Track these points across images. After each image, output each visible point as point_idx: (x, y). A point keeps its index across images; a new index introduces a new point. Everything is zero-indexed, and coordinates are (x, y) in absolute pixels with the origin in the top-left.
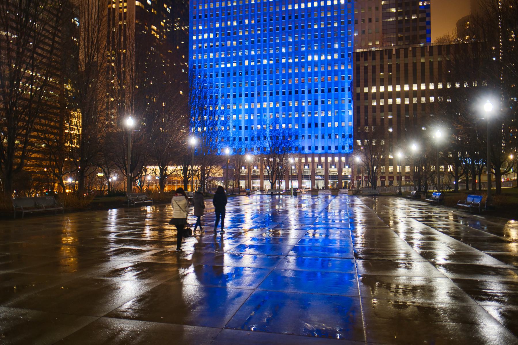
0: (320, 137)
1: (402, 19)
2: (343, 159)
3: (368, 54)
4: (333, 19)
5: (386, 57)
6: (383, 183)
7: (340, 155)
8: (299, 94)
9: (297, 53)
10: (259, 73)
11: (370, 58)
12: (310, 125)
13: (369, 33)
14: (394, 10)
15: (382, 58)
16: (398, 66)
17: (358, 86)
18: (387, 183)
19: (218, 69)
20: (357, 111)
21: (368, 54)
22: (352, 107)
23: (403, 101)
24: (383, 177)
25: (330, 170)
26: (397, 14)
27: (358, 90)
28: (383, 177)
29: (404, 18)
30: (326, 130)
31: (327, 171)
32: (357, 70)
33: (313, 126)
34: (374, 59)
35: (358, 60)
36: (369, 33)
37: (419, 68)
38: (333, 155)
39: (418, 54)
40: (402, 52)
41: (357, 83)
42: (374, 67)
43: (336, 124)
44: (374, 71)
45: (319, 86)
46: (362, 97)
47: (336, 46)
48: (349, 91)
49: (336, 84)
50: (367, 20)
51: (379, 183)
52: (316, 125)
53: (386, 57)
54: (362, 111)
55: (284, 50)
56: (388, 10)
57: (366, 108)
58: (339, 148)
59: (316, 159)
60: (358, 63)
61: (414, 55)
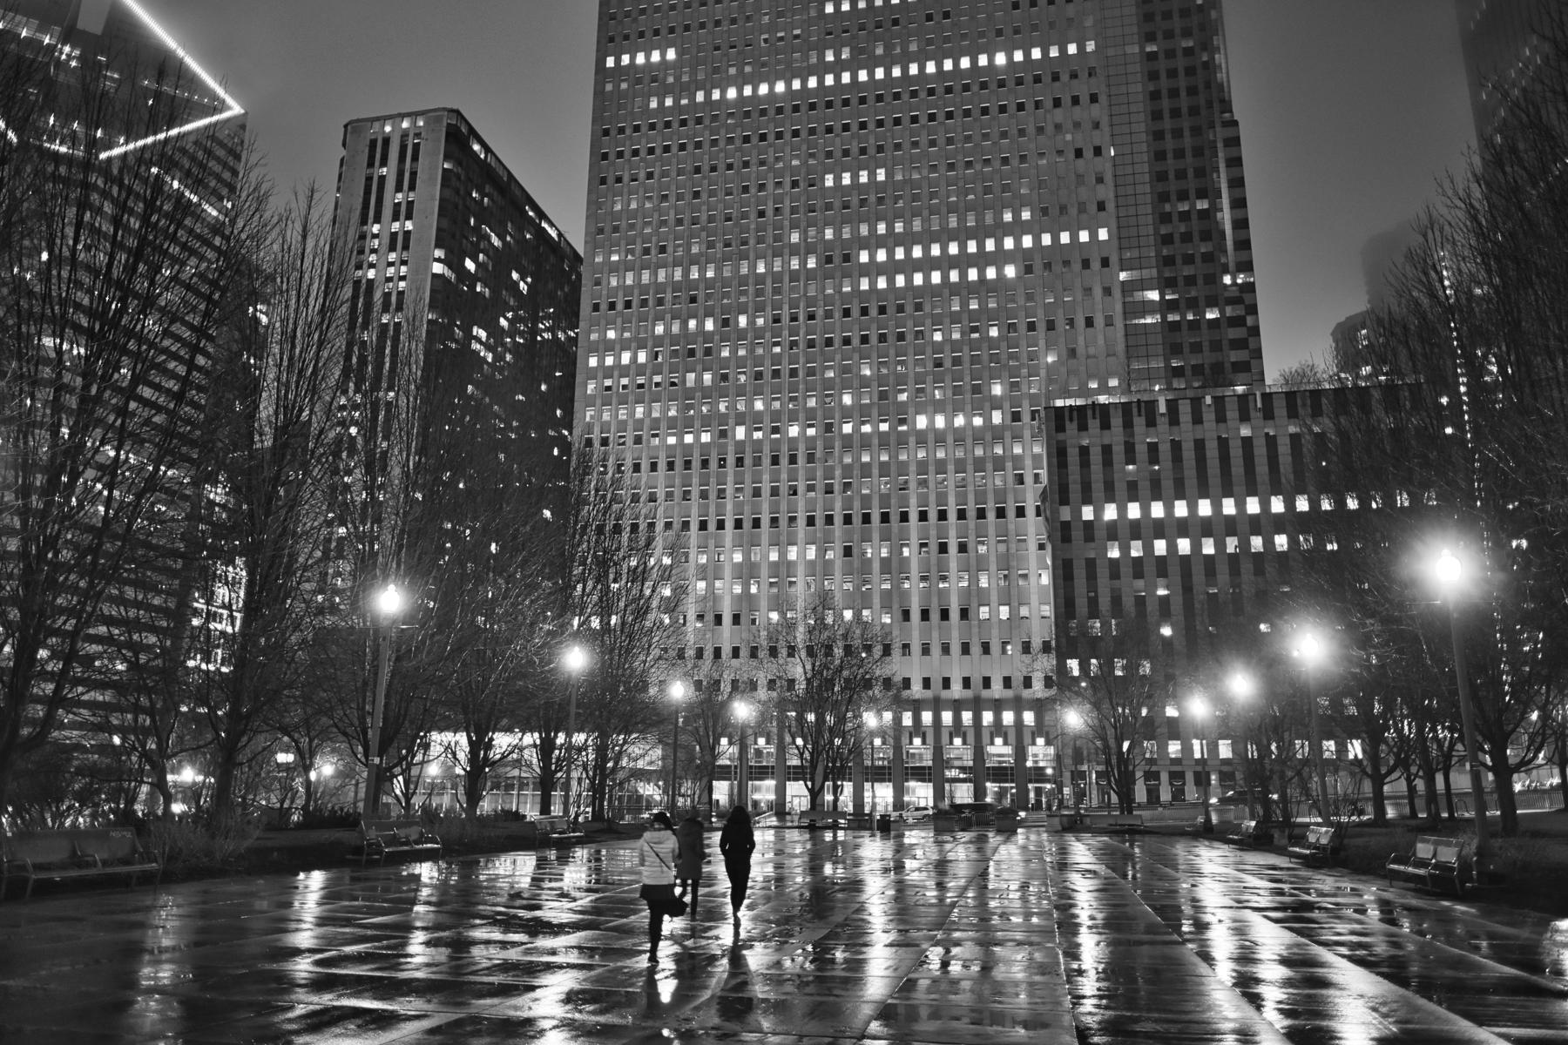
0: (956, 648)
1: (1177, 318)
2: (1029, 717)
3: (1090, 413)
4: (986, 316)
5: (1139, 422)
6: (1153, 794)
7: (1018, 705)
8: (892, 519)
9: (885, 406)
10: (775, 461)
11: (1093, 424)
12: (925, 615)
13: (1088, 357)
14: (1154, 295)
15: (1128, 425)
16: (1176, 446)
17: (1064, 501)
18: (1165, 795)
19: (657, 447)
20: (1064, 573)
21: (1090, 413)
22: (1049, 562)
23: (1197, 546)
24: (1152, 776)
25: (990, 749)
26: (1165, 307)
27: (1065, 514)
28: (1152, 776)
29: (1183, 316)
30: (975, 630)
31: (979, 753)
32: (1059, 455)
33: (935, 616)
34: (1106, 425)
35: (1061, 428)
36: (1088, 357)
37: (1236, 452)
38: (998, 706)
39: (1232, 413)
40: (1185, 408)
41: (1059, 493)
42: (1107, 450)
43: (1004, 612)
44: (1108, 461)
45: (952, 500)
46: (1077, 534)
47: (997, 390)
48: (1038, 515)
49: (1001, 495)
50: (1080, 322)
51: (1140, 794)
52: (945, 615)
53: (1139, 422)
54: (1080, 574)
55: (847, 400)
56: (1138, 296)
57: (1091, 564)
58: (1014, 684)
59: (947, 717)
60: (1061, 436)
61: (1221, 418)
